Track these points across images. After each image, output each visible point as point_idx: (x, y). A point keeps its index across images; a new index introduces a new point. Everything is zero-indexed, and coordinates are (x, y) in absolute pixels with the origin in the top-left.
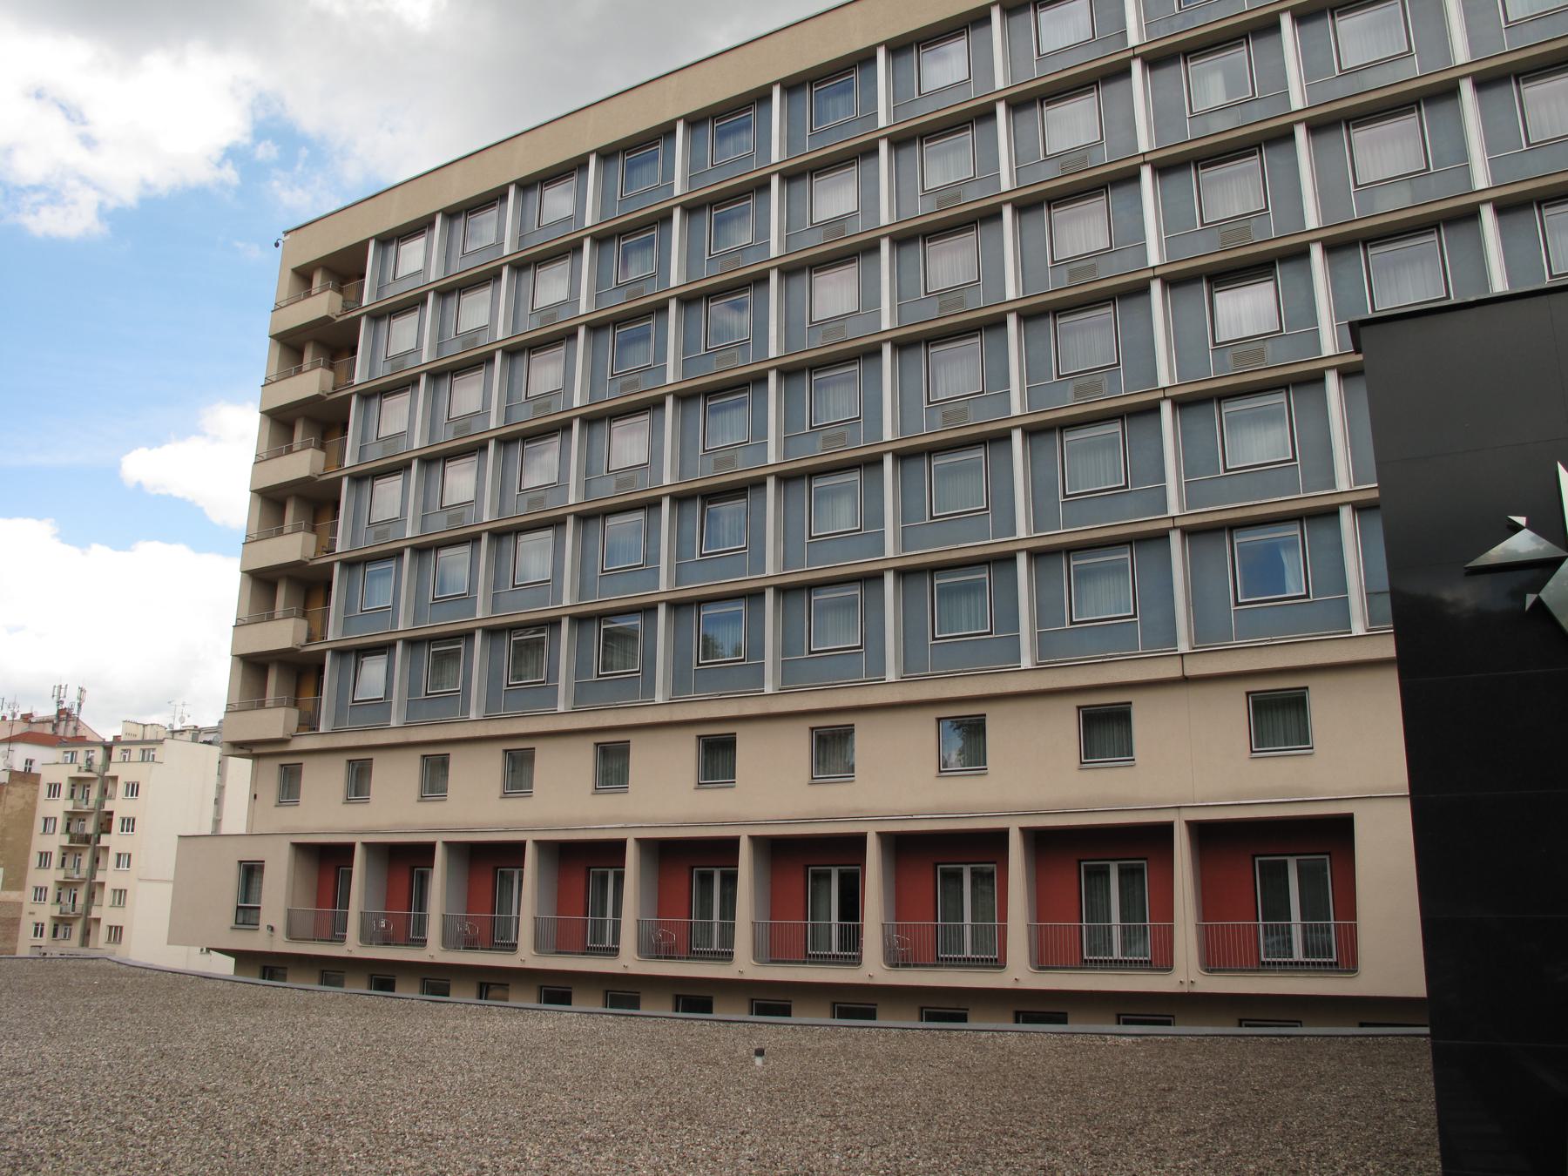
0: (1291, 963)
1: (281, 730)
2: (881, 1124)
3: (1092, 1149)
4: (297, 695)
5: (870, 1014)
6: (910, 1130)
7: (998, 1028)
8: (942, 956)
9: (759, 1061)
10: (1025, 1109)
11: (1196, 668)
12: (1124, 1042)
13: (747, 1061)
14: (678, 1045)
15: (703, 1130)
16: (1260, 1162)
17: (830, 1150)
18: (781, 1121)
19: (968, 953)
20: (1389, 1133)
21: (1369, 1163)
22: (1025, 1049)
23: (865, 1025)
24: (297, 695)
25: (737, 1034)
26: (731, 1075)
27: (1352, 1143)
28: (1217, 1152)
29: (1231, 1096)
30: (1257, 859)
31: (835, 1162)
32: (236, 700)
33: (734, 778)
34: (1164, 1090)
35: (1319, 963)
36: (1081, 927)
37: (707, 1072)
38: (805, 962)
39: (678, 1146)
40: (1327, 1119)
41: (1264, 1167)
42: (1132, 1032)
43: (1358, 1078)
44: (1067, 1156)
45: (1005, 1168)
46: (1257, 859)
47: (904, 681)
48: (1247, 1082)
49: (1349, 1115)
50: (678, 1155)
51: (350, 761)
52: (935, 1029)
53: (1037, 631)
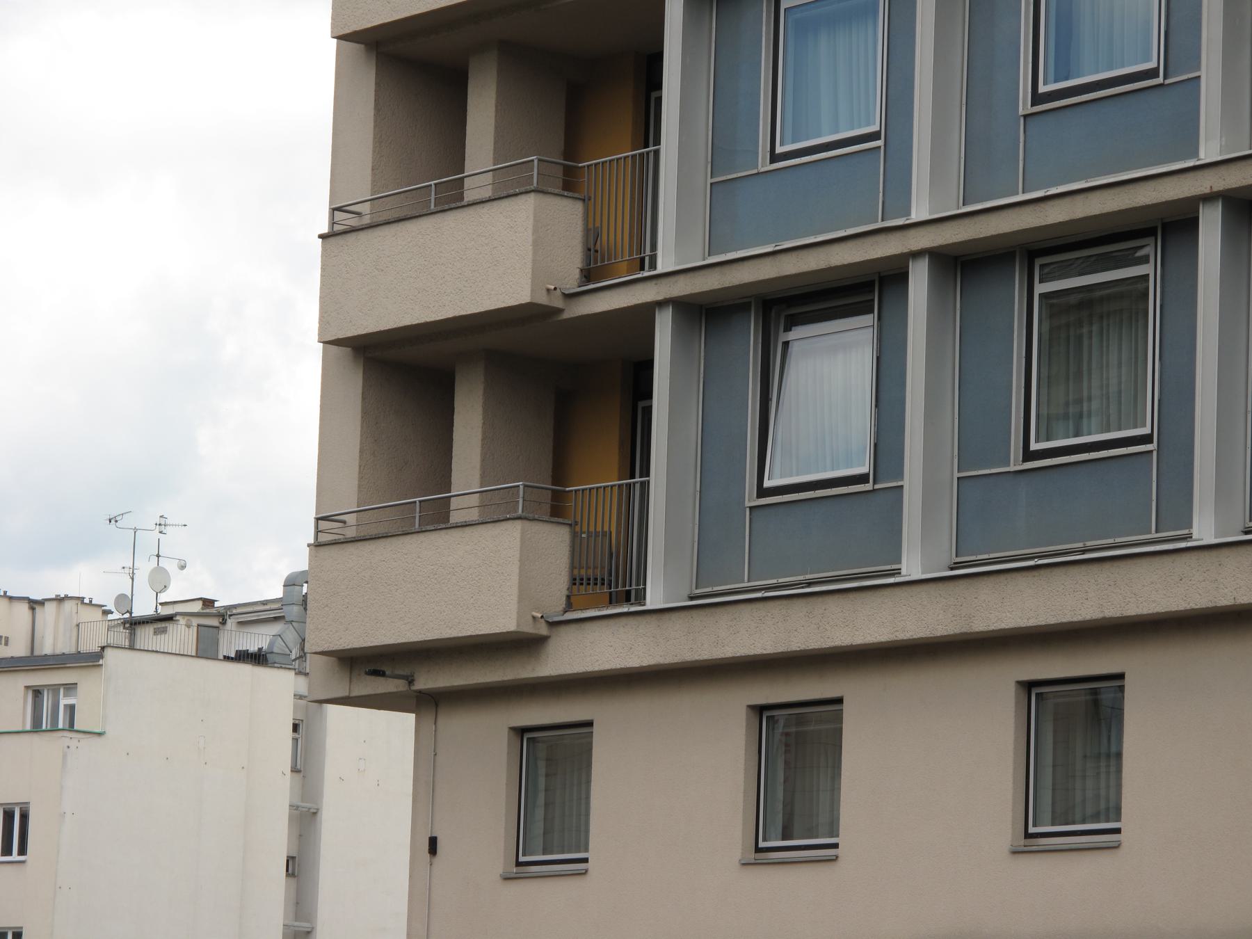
1: (512, 605)
4: (560, 473)
24: (560, 473)
32: (347, 500)
51: (760, 710)
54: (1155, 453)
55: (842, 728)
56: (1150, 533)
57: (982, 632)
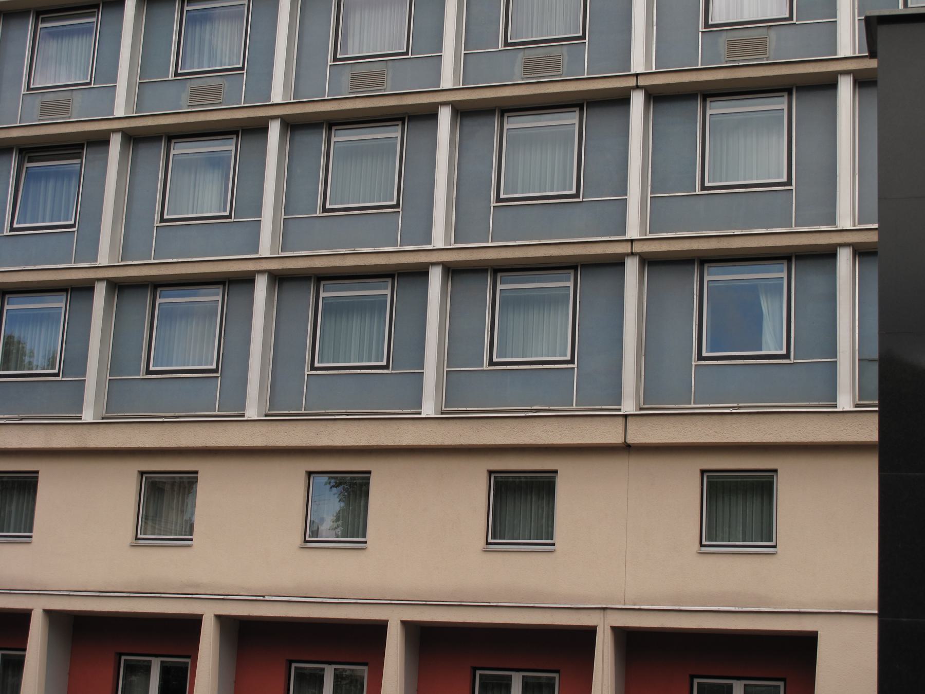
55: (369, 483)
56: (215, 411)
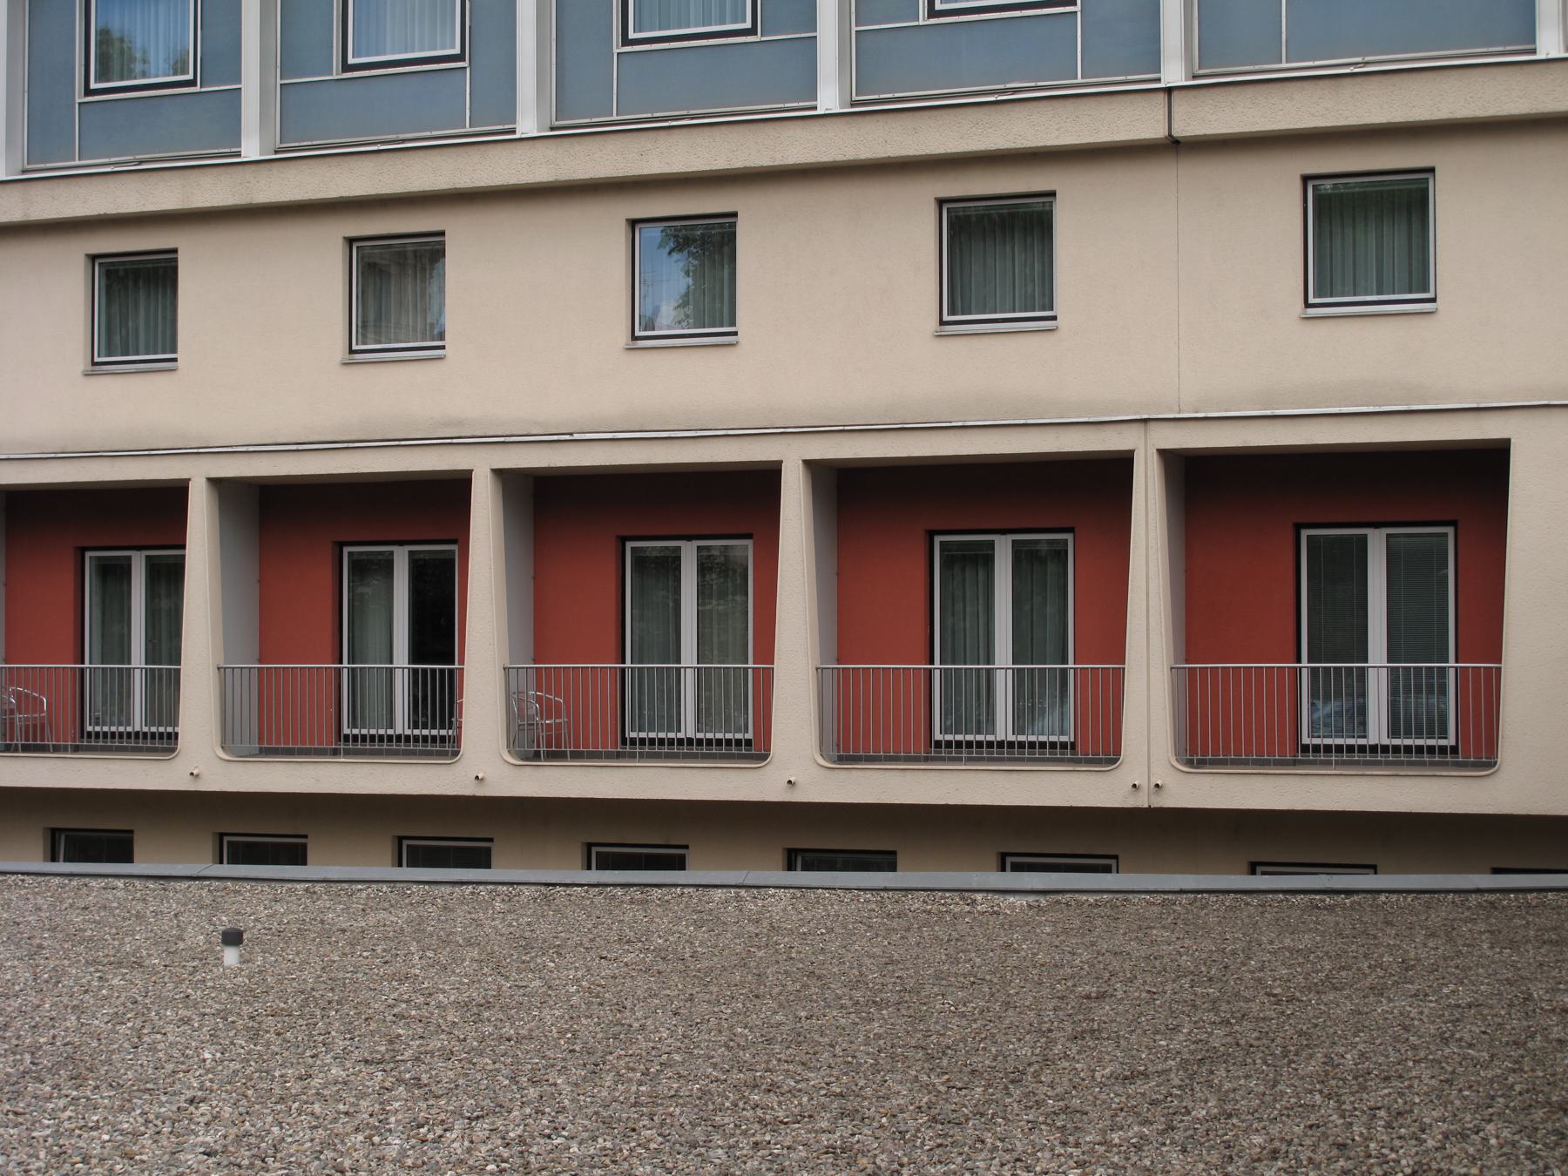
0: (1362, 749)
2: (492, 1075)
3: (934, 1112)
5: (480, 858)
6: (555, 1084)
7: (748, 882)
8: (633, 735)
9: (231, 956)
10: (799, 1038)
11: (1196, 120)
12: (1012, 907)
13: (207, 958)
14: (53, 930)
15: (105, 1097)
16: (1275, 1130)
17: (382, 1128)
18: (277, 1074)
19: (689, 730)
20: (1533, 1070)
21: (1490, 1127)
22: (803, 922)
23: (464, 878)
25: (185, 904)
26: (170, 986)
27: (1460, 1090)
28: (1188, 1113)
29: (1224, 1007)
30: (1305, 533)
31: (392, 1152)
33: (174, 350)
34: (1088, 997)
35: (1420, 749)
36: (930, 672)
37: (115, 982)
38: (335, 753)
39: (48, 1132)
40: (1414, 1048)
41: (1282, 1140)
42: (1029, 887)
43: (1481, 970)
44: (882, 1126)
45: (751, 1153)
46: (1305, 533)
47: (556, 135)
48: (1259, 980)
49: (1460, 1040)
50: (49, 1150)
52: (615, 885)
53: (854, 29)
54: (468, 70)
57: (444, 190)
